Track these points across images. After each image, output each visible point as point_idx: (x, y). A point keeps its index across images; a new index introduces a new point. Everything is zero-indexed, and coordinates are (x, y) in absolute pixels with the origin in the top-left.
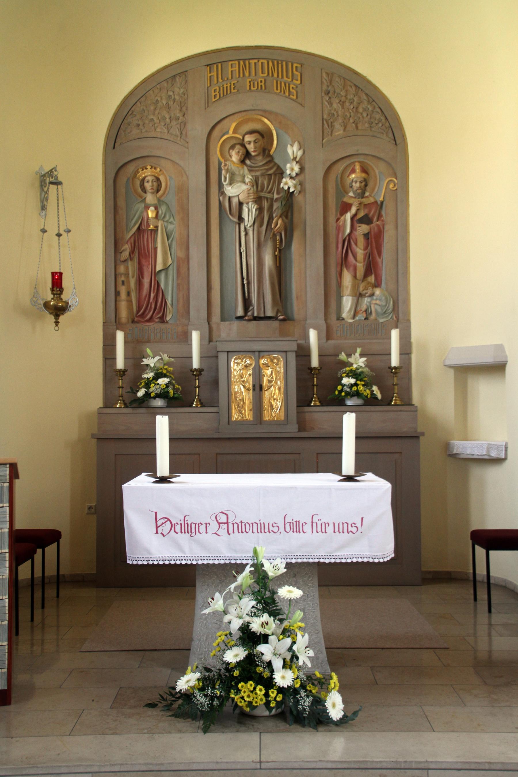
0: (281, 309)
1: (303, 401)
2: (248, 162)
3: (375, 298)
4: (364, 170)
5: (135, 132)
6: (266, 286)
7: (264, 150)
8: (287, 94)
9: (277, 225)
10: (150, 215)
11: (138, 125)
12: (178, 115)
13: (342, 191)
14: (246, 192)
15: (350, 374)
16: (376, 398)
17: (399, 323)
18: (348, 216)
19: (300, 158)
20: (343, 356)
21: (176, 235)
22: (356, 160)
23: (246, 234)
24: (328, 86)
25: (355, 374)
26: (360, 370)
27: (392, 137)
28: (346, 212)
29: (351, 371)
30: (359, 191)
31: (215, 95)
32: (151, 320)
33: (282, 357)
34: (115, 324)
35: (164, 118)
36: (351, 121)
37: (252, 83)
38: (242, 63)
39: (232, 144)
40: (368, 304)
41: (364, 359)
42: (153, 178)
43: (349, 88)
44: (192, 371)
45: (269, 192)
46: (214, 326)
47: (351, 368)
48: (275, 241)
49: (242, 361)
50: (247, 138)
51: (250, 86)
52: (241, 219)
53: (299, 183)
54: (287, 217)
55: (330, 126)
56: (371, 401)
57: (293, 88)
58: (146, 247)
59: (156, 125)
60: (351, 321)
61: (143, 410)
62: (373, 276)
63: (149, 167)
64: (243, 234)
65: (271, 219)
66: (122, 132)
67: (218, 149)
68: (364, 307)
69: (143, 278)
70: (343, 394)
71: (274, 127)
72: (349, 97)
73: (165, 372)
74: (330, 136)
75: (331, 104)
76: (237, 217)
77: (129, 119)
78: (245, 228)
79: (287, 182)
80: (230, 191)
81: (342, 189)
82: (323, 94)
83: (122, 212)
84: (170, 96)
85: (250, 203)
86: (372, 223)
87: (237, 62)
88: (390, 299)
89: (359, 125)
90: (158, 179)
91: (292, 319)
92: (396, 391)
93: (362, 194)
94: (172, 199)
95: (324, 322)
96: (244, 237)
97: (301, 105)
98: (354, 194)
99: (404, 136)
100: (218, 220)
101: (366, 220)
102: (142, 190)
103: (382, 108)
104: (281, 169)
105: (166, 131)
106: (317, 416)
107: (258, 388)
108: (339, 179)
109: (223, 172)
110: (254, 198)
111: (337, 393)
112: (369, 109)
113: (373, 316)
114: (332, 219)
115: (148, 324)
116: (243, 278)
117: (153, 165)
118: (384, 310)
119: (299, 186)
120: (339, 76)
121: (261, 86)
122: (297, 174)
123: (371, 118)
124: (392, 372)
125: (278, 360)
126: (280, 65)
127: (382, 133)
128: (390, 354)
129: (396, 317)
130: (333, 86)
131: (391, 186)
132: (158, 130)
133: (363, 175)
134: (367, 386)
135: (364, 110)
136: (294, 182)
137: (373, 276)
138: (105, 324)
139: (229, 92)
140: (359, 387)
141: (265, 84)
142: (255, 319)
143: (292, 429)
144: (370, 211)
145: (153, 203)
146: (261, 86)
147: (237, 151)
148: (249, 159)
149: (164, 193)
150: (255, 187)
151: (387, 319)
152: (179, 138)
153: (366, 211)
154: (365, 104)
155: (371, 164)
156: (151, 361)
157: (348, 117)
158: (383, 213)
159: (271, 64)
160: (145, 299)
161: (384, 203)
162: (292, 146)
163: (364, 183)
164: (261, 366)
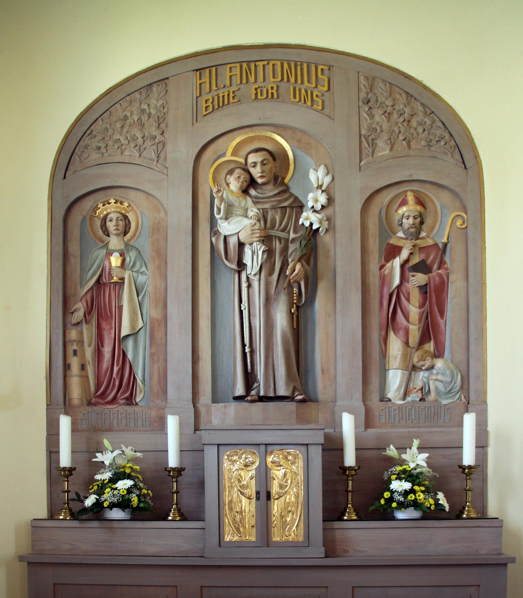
0: (299, 386)
1: (333, 513)
2: (253, 192)
3: (434, 371)
4: (420, 202)
5: (94, 156)
6: (277, 355)
7: (276, 178)
8: (309, 103)
9: (294, 270)
10: (114, 264)
11: (99, 148)
12: (154, 133)
13: (388, 230)
14: (249, 228)
15: (403, 476)
16: (444, 510)
17: (469, 406)
18: (397, 262)
19: (328, 186)
20: (392, 451)
21: (149, 289)
22: (409, 188)
23: (249, 286)
24: (368, 94)
25: (408, 476)
26: (418, 470)
27: (460, 160)
28: (394, 257)
29: (404, 471)
30: (412, 230)
31: (206, 107)
32: (114, 400)
33: (300, 452)
34: (63, 407)
35: (135, 139)
36: (401, 137)
37: (259, 90)
38: (245, 65)
39: (229, 168)
40: (425, 380)
41: (425, 455)
42: (119, 215)
43: (398, 96)
44: (168, 470)
45: (283, 231)
46: (202, 410)
47: (404, 467)
48: (290, 294)
49: (240, 458)
50: (252, 159)
51: (256, 94)
52: (241, 265)
53: (325, 219)
54: (308, 263)
55: (371, 145)
56: (434, 514)
57: (317, 96)
58: (108, 306)
59: (123, 147)
60: (402, 402)
61: (95, 524)
62: (432, 343)
63: (112, 201)
64: (244, 285)
65: (284, 264)
66: (77, 156)
67: (211, 176)
69: (103, 346)
70: (394, 505)
71: (290, 146)
72: (397, 107)
73: (128, 471)
74: (370, 157)
75: (372, 117)
76: (236, 263)
77: (86, 141)
78: (248, 278)
79: (308, 216)
80: (226, 228)
81: (387, 227)
82: (360, 104)
83: (75, 262)
84: (143, 111)
85: (255, 244)
86: (431, 272)
87: (238, 65)
88: (457, 373)
89: (412, 143)
90: (125, 217)
91: (316, 401)
92: (469, 499)
93: (416, 233)
94: (144, 243)
95: (362, 404)
96: (246, 289)
97: (330, 117)
98: (404, 234)
99: (477, 157)
100: (209, 268)
101: (423, 267)
102: (104, 232)
103: (445, 123)
104: (300, 201)
105: (137, 155)
106: (352, 534)
107: (264, 496)
108: (383, 213)
109: (217, 202)
110: (260, 237)
111: (382, 502)
112: (426, 123)
113: (432, 396)
114: (373, 266)
116: (244, 345)
117: (118, 198)
118: (449, 389)
119: (327, 222)
120: (384, 81)
121: (272, 93)
122: (323, 207)
123: (429, 134)
124: (463, 472)
125: (295, 457)
126: (299, 68)
127: (446, 153)
128: (461, 448)
129: (465, 398)
130: (375, 94)
131: (459, 223)
132: (126, 153)
133: (419, 208)
134: (429, 493)
135: (420, 124)
136: (319, 216)
137: (432, 343)
138: (50, 407)
139: (226, 103)
140: (417, 495)
141: (277, 91)
142: (262, 399)
143: (316, 552)
144: (428, 256)
145: (118, 248)
146: (272, 93)
147: (237, 176)
148: (255, 189)
149: (134, 235)
150: (262, 222)
151: (452, 401)
152: (155, 163)
153: (423, 256)
154: (420, 116)
155: (431, 195)
156: (106, 458)
157: (396, 133)
158: (447, 259)
159: (286, 66)
161: (448, 245)
162: (316, 170)
163: (419, 220)
164: (269, 465)
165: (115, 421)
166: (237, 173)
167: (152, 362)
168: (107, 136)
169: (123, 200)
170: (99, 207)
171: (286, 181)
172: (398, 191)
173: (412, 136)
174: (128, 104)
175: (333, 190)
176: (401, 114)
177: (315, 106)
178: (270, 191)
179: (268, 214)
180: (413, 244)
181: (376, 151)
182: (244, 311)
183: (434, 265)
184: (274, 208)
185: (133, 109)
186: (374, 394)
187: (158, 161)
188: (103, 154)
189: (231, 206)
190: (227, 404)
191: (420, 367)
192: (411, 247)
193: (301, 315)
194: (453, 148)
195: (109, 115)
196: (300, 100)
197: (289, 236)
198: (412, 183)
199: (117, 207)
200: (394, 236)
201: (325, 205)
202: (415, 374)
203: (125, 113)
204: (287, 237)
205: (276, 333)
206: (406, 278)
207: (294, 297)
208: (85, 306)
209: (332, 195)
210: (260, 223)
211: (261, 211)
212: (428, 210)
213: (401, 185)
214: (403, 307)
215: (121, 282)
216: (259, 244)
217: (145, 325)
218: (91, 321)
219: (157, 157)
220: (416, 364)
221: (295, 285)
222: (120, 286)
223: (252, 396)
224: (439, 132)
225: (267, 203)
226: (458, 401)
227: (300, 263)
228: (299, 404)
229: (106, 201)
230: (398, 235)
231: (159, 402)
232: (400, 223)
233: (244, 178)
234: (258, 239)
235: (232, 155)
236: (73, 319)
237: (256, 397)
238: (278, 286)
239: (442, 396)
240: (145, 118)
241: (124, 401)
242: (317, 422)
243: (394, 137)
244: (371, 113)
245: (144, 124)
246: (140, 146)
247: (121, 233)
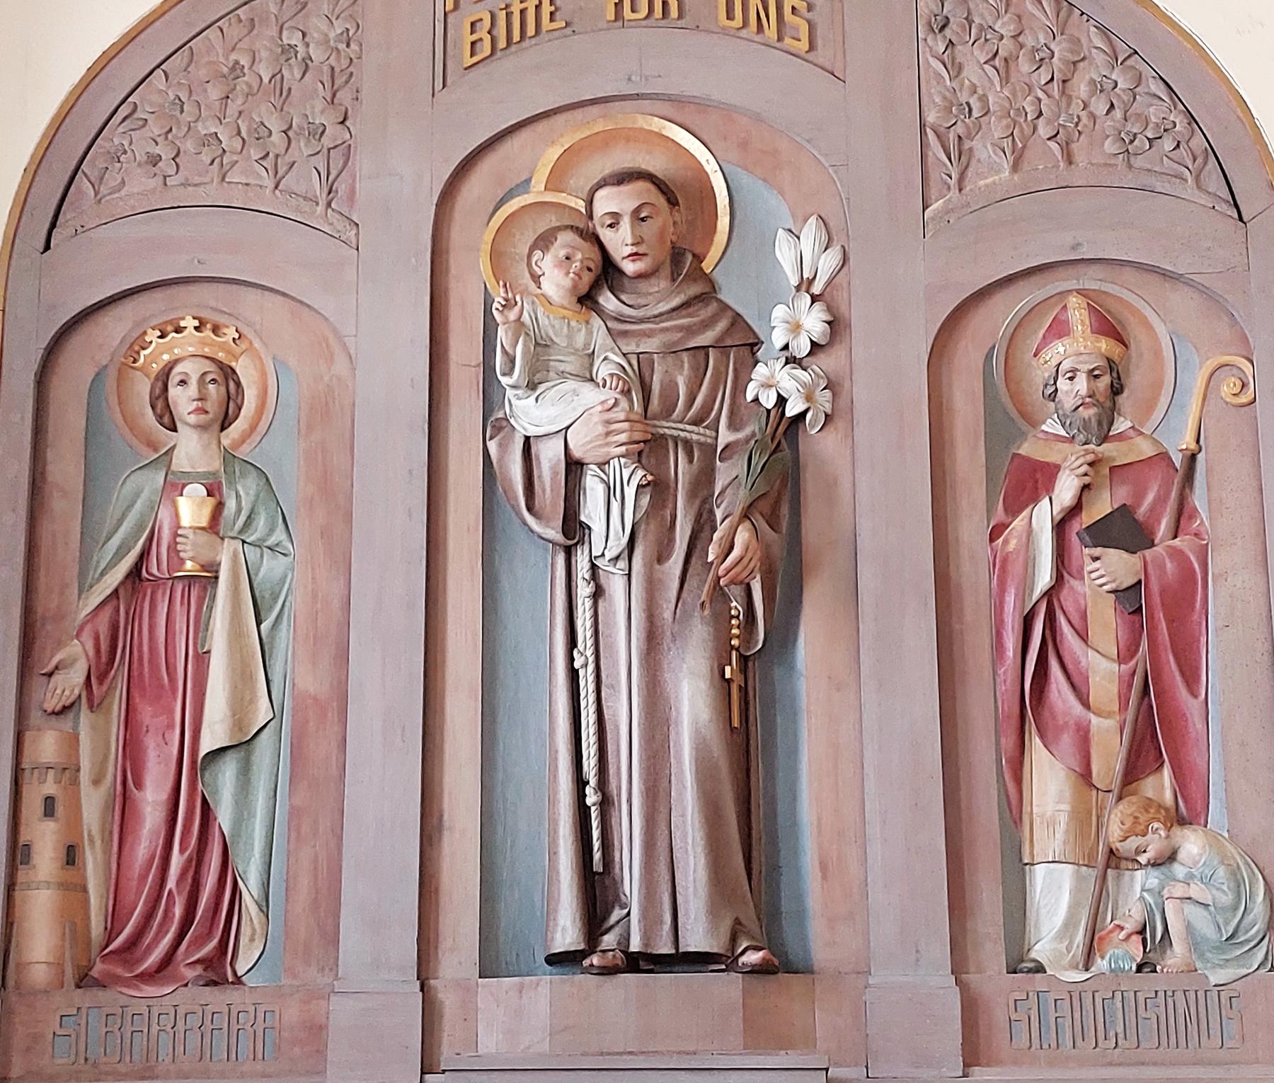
2: (608, 301)
3: (1179, 870)
4: (1108, 326)
5: (140, 183)
7: (677, 256)
8: (771, 32)
9: (731, 548)
10: (186, 520)
11: (155, 160)
13: (1014, 413)
18: (1043, 516)
21: (298, 602)
22: (1073, 285)
23: (598, 594)
27: (1225, 194)
28: (1035, 500)
35: (261, 133)
36: (1044, 131)
39: (542, 227)
45: (697, 422)
46: (448, 998)
48: (721, 619)
50: (607, 201)
52: (574, 529)
54: (773, 524)
58: (146, 649)
62: (1167, 771)
63: (189, 323)
64: (584, 591)
65: (703, 526)
68: (1132, 914)
69: (139, 785)
72: (1028, 40)
74: (954, 193)
75: (956, 69)
77: (116, 137)
78: (594, 567)
80: (531, 414)
81: (1009, 412)
83: (64, 510)
90: (228, 373)
91: (808, 970)
93: (1100, 423)
94: (283, 454)
96: (589, 603)
101: (1123, 530)
102: (160, 418)
105: (269, 183)
114: (971, 527)
115: (150, 990)
116: (580, 783)
119: (828, 393)
131: (1228, 388)
133: (1104, 344)
135: (1097, 88)
137: (1167, 771)
139: (531, 30)
142: (635, 963)
144: (1139, 495)
147: (562, 253)
149: (253, 428)
152: (320, 209)
153: (1123, 495)
158: (1199, 499)
160: (143, 878)
161: (1201, 457)
163: (1106, 380)
165: (165, 1039)
166: (564, 246)
167: (293, 835)
168: (178, 122)
169: (221, 319)
170: (148, 339)
171: (707, 266)
172: (1041, 294)
173: (1077, 125)
174: (245, 31)
176: (1042, 60)
177: (788, 41)
178: (661, 297)
180: (1090, 458)
181: (970, 173)
182: (581, 673)
183: (1160, 523)
184: (672, 351)
185: (257, 45)
186: (988, 946)
187: (329, 205)
188: (165, 177)
191: (1132, 855)
192: (1085, 468)
193: (756, 682)
194: (1200, 160)
195: (186, 60)
196: (745, 24)
197: (716, 438)
198: (1081, 269)
199: (203, 343)
200: (1032, 432)
202: (1119, 877)
203: (233, 57)
205: (679, 744)
206: (1075, 564)
207: (732, 627)
208: (91, 653)
209: (843, 308)
210: (631, 401)
211: (635, 363)
212: (1133, 346)
213: (1048, 275)
214: (1067, 660)
215: (208, 578)
217: (277, 715)
218: (105, 703)
219: (326, 190)
220: (1118, 845)
221: (736, 592)
222: (205, 589)
223: (604, 951)
224: (1155, 113)
225: (648, 334)
226: (1262, 971)
227: (747, 524)
229: (170, 322)
230: (1044, 427)
231: (312, 975)
232: (1050, 390)
234: (623, 449)
236: (49, 695)
237: (619, 954)
238: (684, 595)
239: (1209, 955)
240: (292, 74)
241: (199, 970)
242: (809, 1042)
243: (1022, 130)
244: (953, 59)
245: (290, 89)
246: (277, 156)
247: (213, 421)
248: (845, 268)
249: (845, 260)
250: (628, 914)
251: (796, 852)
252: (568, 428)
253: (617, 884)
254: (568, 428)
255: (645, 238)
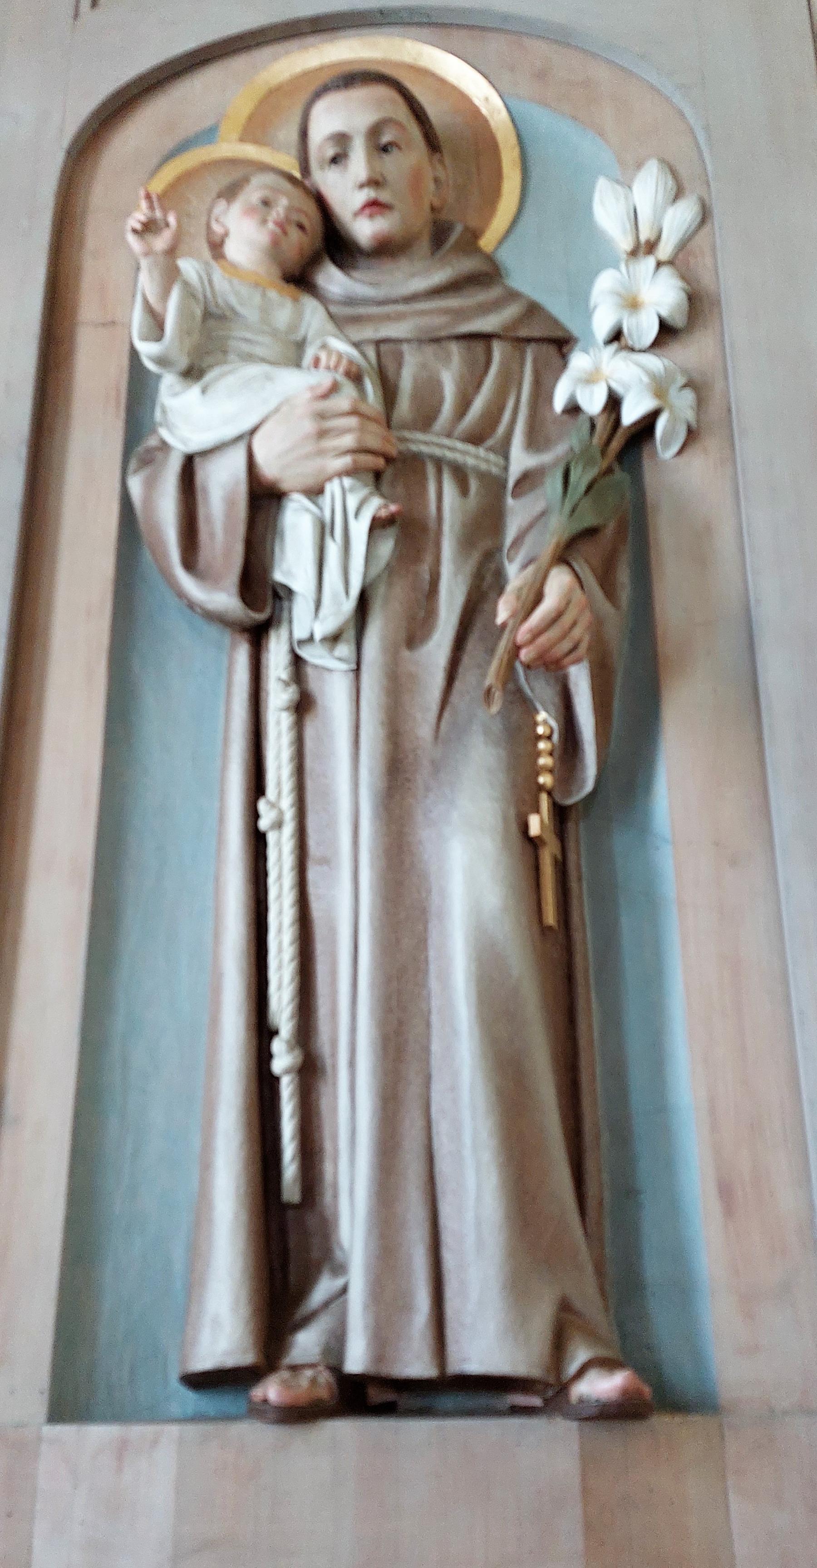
2: (333, 279)
6: (454, 1089)
7: (439, 234)
9: (538, 598)
19: (683, 245)
23: (303, 706)
45: (476, 438)
48: (519, 736)
50: (330, 118)
52: (262, 599)
53: (681, 380)
64: (278, 697)
78: (297, 662)
80: (190, 417)
85: (333, 488)
116: (262, 1031)
142: (359, 1396)
171: (487, 242)
175: (708, 261)
179: (400, 365)
182: (271, 838)
189: (222, 318)
190: (137, 1431)
193: (581, 861)
197: (506, 469)
201: (679, 321)
204: (495, 470)
207: (538, 754)
209: (706, 280)
211: (371, 353)
216: (352, 489)
221: (541, 691)
223: (295, 1368)
225: (400, 317)
228: (610, 1439)
233: (289, 209)
235: (242, 140)
238: (455, 698)
248: (706, 230)
249: (705, 215)
250: (344, 1290)
251: (668, 1164)
252: (253, 431)
253: (326, 1229)
254: (253, 431)
255: (390, 178)
